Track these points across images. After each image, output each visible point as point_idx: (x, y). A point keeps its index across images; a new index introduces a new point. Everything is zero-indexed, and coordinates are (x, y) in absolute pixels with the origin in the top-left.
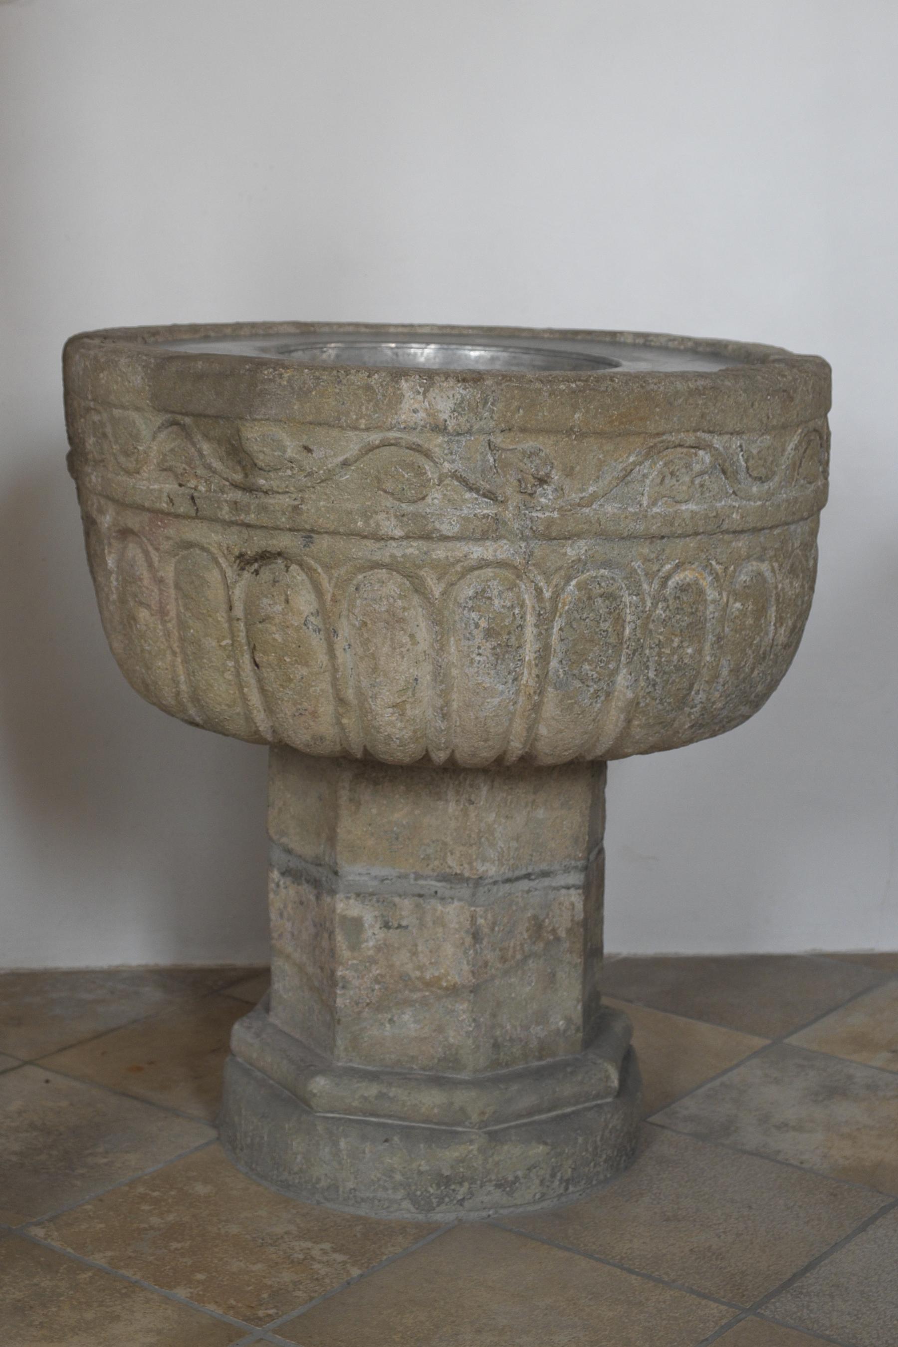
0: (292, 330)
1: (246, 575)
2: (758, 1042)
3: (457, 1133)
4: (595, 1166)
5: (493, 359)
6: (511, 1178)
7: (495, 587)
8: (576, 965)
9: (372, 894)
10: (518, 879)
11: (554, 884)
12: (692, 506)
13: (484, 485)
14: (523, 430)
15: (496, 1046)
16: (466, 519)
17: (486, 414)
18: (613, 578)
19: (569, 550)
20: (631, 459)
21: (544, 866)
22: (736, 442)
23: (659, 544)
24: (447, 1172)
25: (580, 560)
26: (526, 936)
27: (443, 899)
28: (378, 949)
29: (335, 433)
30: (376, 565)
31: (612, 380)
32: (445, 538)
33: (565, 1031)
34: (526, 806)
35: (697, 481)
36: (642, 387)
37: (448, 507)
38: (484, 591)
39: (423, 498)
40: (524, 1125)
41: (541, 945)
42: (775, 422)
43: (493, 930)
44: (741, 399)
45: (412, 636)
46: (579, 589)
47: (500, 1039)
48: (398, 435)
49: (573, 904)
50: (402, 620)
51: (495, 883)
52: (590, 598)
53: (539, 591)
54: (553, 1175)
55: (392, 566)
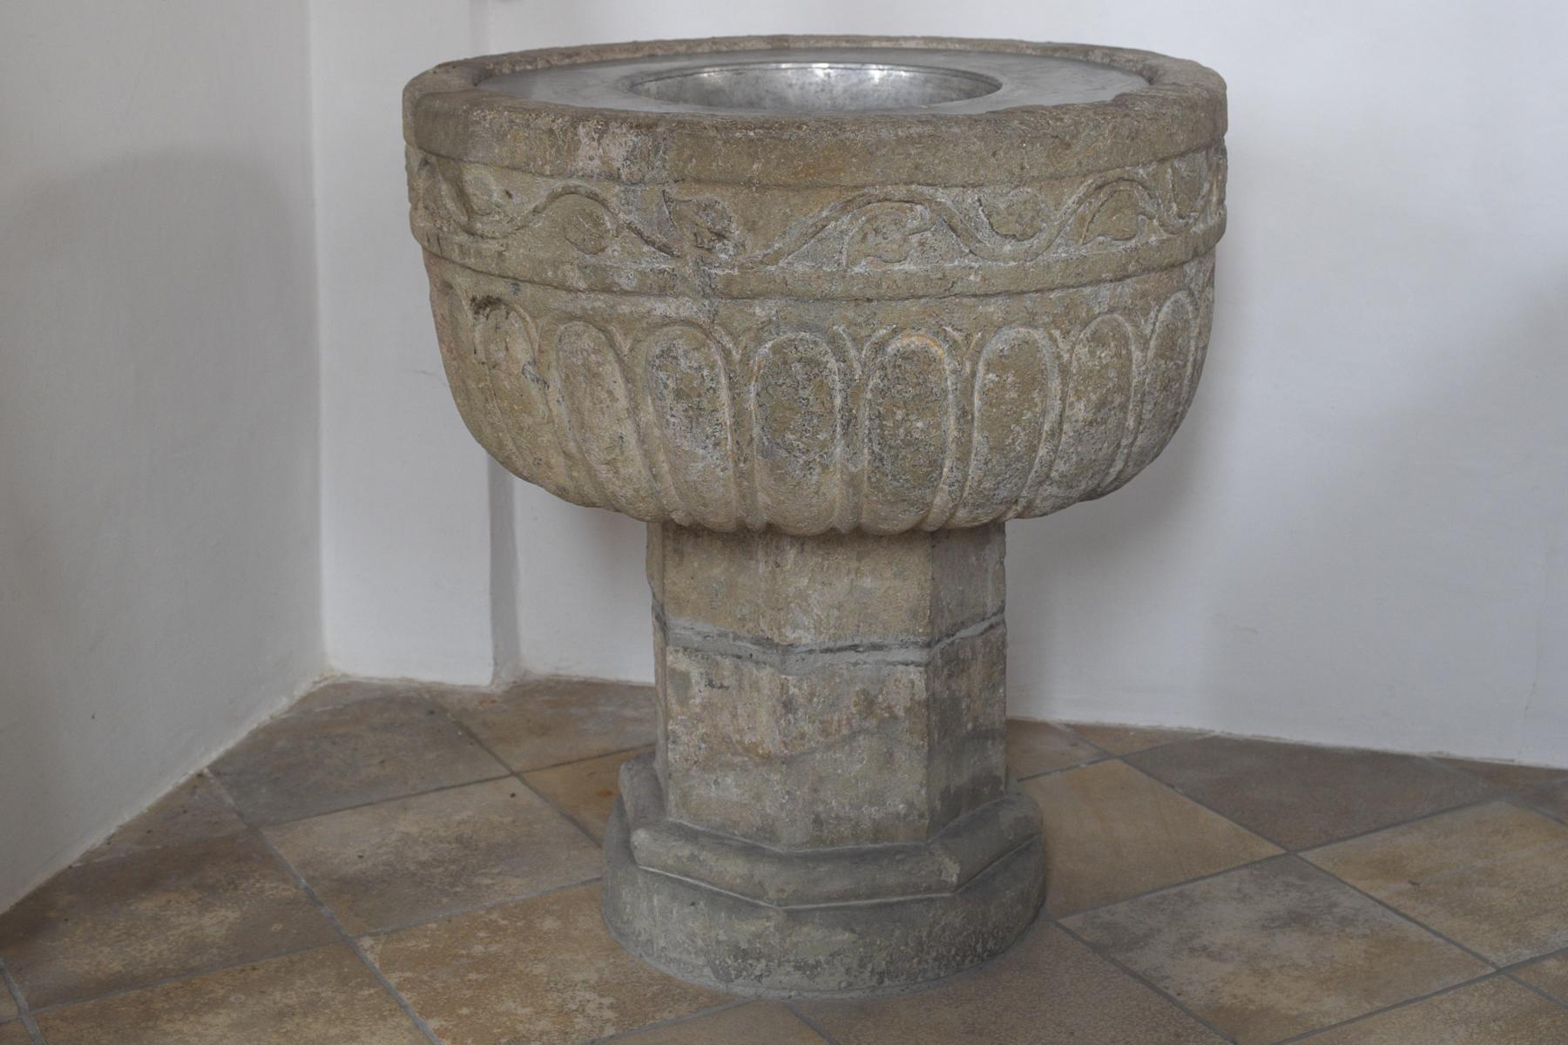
0: (763, 46)
1: (482, 319)
2: (1270, 849)
3: (757, 906)
4: (919, 963)
5: (911, 81)
6: (811, 961)
7: (681, 346)
8: (917, 748)
9: (697, 650)
10: (841, 649)
11: (889, 659)
12: (909, 266)
13: (659, 238)
14: (698, 181)
15: (818, 821)
16: (643, 273)
17: (658, 163)
18: (815, 343)
19: (758, 310)
20: (825, 214)
21: (875, 639)
22: (971, 197)
23: (868, 309)
24: (744, 946)
25: (770, 321)
26: (854, 710)
27: (757, 663)
28: (704, 707)
29: (528, 178)
30: (572, 317)
31: (799, 128)
32: (625, 293)
33: (905, 816)
34: (849, 572)
35: (915, 239)
36: (835, 135)
37: (629, 263)
38: (669, 349)
39: (603, 250)
40: (836, 908)
41: (875, 722)
42: (1035, 173)
43: (810, 701)
44: (974, 149)
45: (610, 393)
46: (774, 353)
47: (823, 816)
48: (577, 182)
49: (912, 682)
50: (596, 375)
51: (811, 652)
52: (785, 363)
53: (727, 354)
54: (862, 965)
55: (586, 318)
